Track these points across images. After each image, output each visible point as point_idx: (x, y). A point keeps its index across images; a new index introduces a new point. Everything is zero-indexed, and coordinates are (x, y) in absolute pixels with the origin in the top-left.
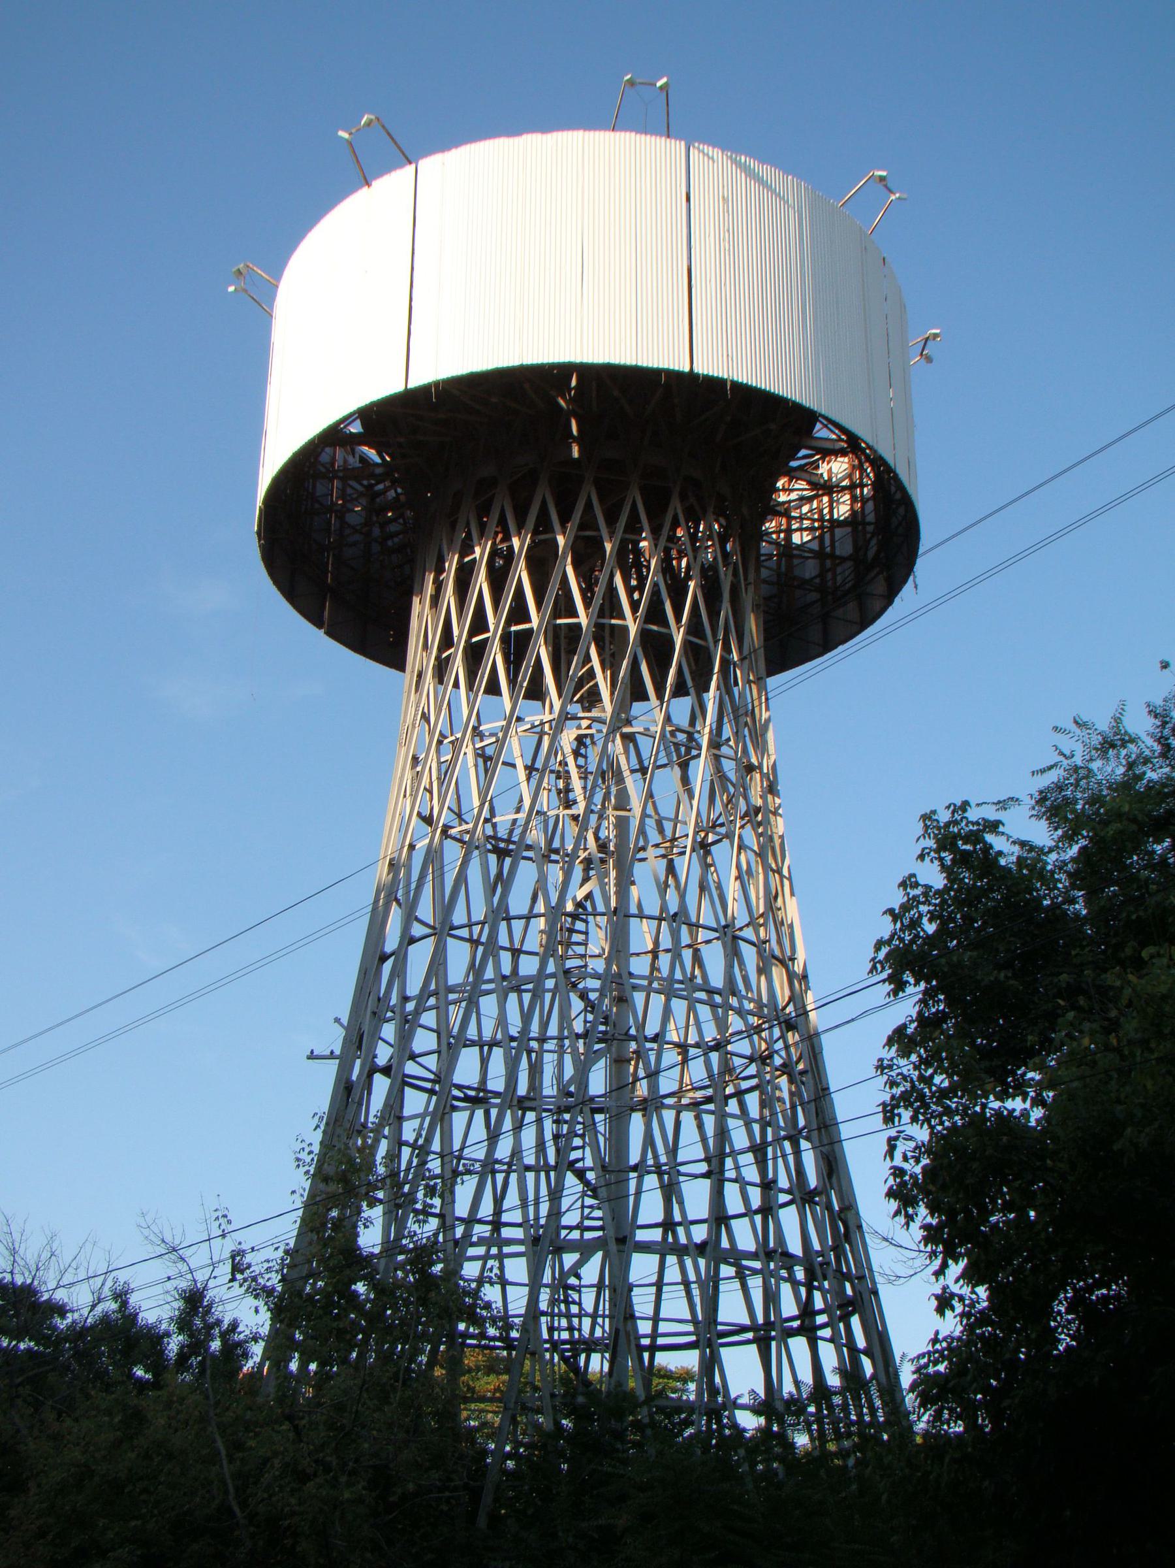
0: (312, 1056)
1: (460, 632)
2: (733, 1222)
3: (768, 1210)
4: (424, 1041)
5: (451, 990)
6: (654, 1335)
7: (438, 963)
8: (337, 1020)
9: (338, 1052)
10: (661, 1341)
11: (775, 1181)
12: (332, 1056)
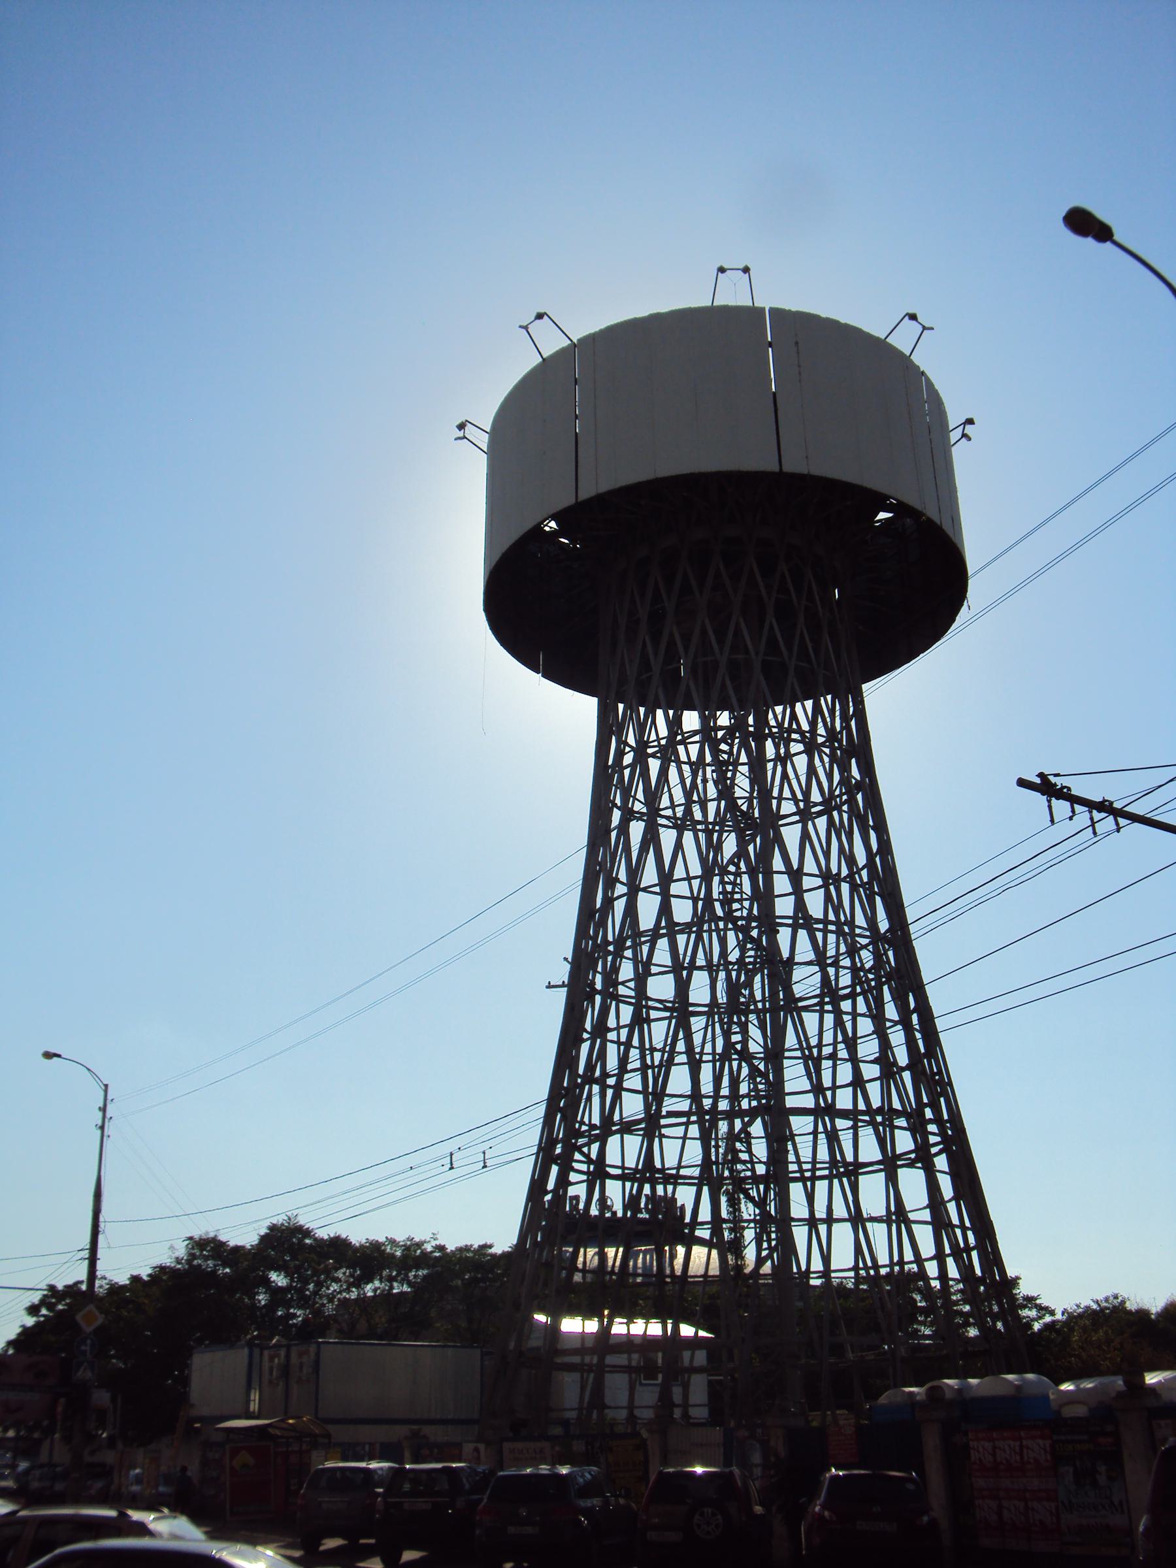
0: (549, 986)
4: (627, 971)
6: (814, 1170)
7: (631, 911)
8: (566, 959)
12: (563, 985)
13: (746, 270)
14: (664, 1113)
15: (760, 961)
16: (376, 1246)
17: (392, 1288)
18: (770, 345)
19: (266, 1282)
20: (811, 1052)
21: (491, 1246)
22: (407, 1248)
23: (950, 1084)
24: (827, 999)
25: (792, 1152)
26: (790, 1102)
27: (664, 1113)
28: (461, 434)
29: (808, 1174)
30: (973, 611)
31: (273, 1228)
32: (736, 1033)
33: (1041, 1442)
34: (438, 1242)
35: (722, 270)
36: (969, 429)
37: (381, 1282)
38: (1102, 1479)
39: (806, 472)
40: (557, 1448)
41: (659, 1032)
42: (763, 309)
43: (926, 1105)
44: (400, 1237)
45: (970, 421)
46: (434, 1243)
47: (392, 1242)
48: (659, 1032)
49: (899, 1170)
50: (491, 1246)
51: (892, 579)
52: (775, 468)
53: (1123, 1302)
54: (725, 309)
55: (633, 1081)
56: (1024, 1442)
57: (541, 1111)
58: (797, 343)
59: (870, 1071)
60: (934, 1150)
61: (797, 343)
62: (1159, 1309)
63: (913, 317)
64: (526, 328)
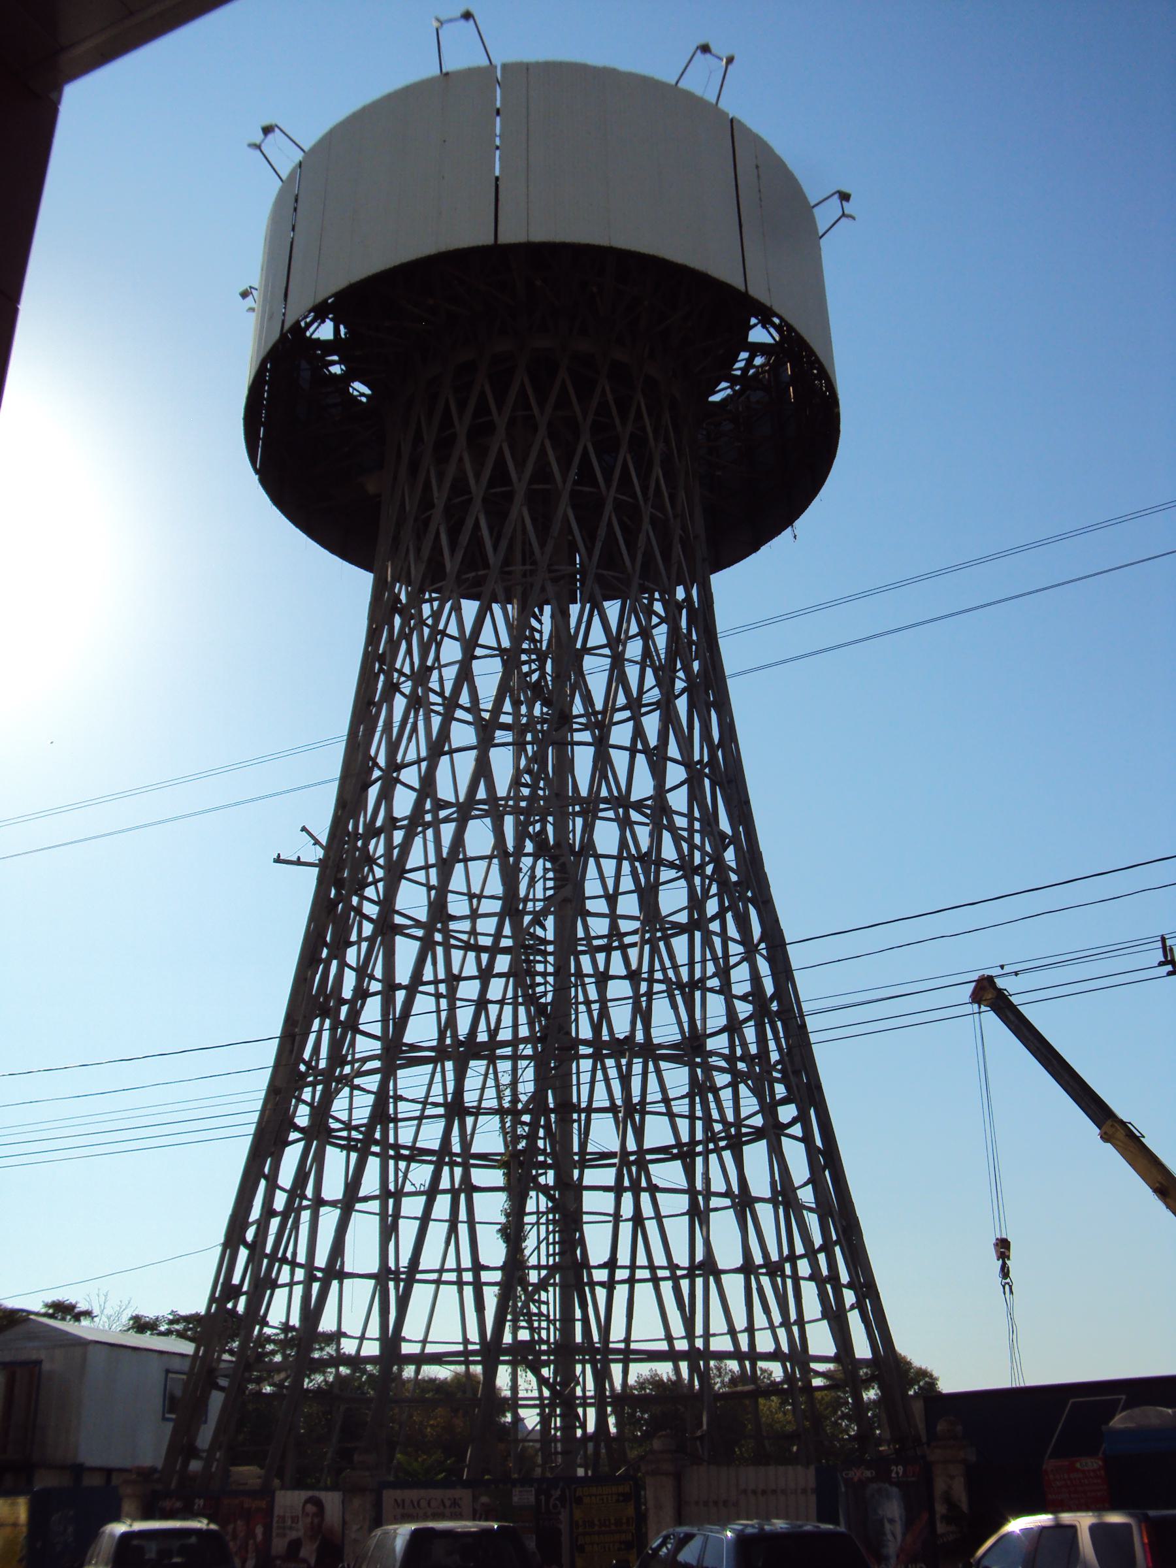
0: (278, 860)
1: (440, 498)
13: (467, 16)
18: (498, 148)
20: (677, 974)
26: (593, 980)
32: (506, 937)
41: (406, 951)
43: (836, 1243)
48: (406, 951)
49: (585, 1193)
52: (433, 1217)
55: (372, 1010)
59: (744, 1009)
64: (258, 147)
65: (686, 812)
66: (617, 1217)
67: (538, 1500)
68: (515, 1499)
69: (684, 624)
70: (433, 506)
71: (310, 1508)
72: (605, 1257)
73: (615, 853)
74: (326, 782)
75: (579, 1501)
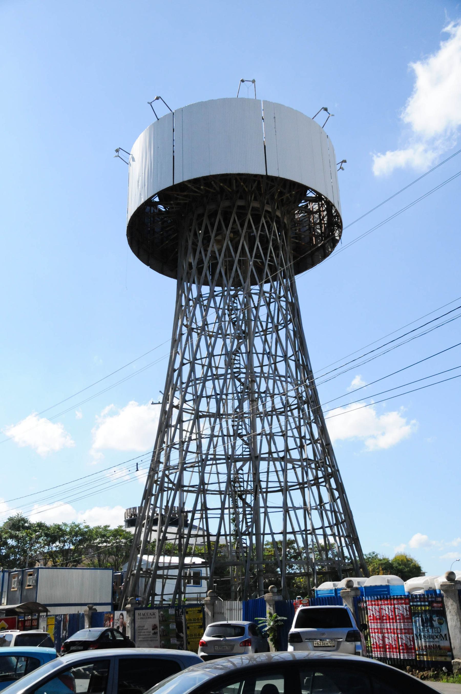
2: (291, 451)
3: (302, 447)
5: (197, 379)
6: (267, 488)
8: (160, 392)
9: (161, 402)
10: (269, 490)
11: (305, 436)
12: (159, 403)
13: (254, 81)
14: (209, 459)
15: (250, 395)
16: (58, 528)
17: (64, 545)
19: (6, 543)
21: (109, 526)
22: (72, 527)
23: (338, 471)
24: (274, 413)
25: (17, 570)
27: (209, 459)
28: (117, 154)
29: (264, 490)
30: (343, 245)
31: (11, 519)
33: (404, 606)
34: (86, 524)
35: (243, 81)
36: (344, 165)
37: (60, 543)
38: (436, 624)
39: (277, 176)
40: (162, 613)
42: (260, 101)
44: (69, 522)
45: (345, 161)
46: (84, 524)
47: (65, 525)
50: (109, 526)
51: (253, 83)
53: (376, 555)
54: (243, 100)
56: (396, 606)
57: (152, 454)
58: (275, 117)
60: (323, 480)
61: (275, 117)
62: (392, 559)
63: (326, 110)
64: (150, 104)
65: (175, 398)
66: (223, 508)
67: (176, 613)
68: (170, 612)
69: (228, 301)
70: (203, 263)
71: (121, 617)
72: (281, 529)
73: (262, 352)
74: (349, 226)
75: (187, 613)
